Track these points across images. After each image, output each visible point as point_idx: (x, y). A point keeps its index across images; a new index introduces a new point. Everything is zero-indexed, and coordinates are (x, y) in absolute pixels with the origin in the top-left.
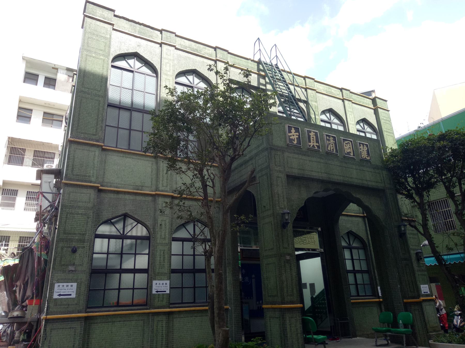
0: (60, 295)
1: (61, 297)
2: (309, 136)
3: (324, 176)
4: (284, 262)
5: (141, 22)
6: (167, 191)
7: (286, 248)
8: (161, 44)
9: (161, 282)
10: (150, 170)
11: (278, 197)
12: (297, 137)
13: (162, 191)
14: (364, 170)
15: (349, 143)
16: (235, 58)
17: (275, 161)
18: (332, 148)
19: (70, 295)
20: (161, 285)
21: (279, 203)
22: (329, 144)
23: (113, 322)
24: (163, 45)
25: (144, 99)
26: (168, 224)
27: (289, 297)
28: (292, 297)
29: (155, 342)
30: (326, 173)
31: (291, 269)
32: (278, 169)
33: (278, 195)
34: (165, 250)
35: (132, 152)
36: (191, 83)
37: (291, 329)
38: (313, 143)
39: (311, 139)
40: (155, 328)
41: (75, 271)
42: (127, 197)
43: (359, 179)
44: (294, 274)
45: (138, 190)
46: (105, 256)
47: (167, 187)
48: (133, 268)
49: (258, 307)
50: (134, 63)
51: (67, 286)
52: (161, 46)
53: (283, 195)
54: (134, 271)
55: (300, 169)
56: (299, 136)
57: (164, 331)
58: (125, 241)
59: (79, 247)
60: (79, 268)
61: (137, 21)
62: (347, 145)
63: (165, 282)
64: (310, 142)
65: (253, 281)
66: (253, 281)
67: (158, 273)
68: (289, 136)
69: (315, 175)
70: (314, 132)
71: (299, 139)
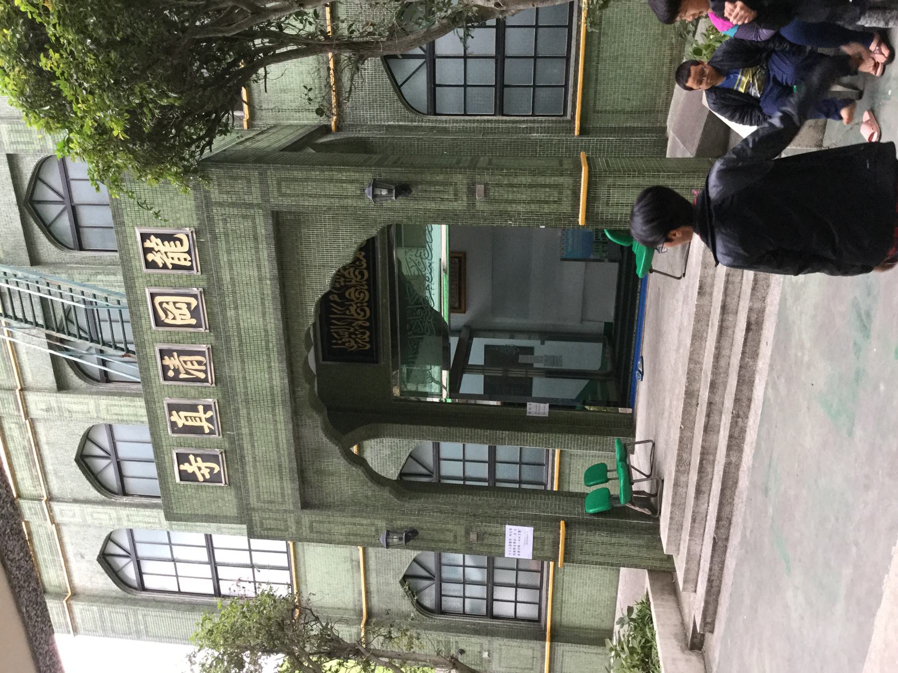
2: (187, 429)
3: (282, 415)
4: (482, 545)
7: (455, 537)
12: (199, 459)
15: (161, 304)
25: (113, 336)
27: (546, 547)
28: (546, 542)
30: (273, 409)
32: (294, 528)
33: (349, 534)
37: (601, 555)
39: (190, 423)
41: (489, 651)
42: (373, 580)
59: (457, 647)
60: (486, 647)
62: (171, 316)
69: (284, 435)
70: (171, 415)
71: (206, 458)
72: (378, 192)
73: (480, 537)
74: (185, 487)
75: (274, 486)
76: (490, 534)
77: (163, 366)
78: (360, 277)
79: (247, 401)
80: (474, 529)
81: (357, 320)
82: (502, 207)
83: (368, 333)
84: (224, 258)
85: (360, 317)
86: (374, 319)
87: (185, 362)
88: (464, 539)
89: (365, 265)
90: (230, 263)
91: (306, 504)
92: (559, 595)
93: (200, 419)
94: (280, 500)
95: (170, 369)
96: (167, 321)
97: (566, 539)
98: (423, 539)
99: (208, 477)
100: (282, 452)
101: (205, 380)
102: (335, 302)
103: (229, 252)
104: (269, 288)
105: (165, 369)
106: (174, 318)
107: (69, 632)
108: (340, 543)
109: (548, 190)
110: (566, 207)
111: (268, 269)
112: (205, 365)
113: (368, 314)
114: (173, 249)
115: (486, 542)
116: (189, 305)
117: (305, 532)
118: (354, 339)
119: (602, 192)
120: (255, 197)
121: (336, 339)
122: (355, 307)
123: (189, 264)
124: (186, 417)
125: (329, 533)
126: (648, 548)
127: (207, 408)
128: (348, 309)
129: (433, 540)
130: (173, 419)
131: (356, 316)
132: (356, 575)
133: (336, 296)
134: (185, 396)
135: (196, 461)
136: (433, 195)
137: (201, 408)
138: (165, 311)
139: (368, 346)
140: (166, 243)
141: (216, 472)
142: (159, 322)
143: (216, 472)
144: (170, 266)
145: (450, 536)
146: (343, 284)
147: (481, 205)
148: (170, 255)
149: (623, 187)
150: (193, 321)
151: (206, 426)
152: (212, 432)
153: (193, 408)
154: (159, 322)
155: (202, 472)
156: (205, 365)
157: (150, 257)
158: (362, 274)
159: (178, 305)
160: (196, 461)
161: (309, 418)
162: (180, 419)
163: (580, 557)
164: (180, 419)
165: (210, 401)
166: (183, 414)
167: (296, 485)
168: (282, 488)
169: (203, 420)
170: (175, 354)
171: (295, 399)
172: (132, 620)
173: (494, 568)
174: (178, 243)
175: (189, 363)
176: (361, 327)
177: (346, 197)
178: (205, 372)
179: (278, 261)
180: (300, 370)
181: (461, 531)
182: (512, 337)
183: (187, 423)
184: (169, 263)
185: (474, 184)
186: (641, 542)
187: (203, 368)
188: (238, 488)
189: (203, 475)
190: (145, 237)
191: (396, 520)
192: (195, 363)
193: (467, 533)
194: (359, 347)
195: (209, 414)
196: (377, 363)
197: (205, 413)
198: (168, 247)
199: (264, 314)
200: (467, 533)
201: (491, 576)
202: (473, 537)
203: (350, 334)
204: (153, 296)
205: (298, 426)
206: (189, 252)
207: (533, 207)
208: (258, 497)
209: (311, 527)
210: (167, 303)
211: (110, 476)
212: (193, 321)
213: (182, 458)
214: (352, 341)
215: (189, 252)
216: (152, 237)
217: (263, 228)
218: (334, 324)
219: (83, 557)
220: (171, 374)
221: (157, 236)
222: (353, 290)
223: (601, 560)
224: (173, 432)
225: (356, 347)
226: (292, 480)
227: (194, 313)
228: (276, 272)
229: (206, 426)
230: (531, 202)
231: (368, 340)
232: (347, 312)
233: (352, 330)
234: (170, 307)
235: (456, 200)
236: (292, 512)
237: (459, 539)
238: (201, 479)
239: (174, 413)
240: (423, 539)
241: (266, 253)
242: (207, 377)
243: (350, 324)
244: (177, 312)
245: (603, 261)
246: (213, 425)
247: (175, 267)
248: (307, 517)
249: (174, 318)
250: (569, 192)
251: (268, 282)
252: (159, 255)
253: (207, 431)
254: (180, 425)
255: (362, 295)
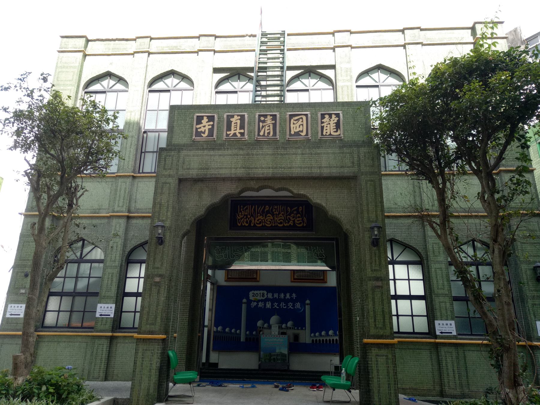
0: (11, 315)
1: (13, 316)
3: (241, 172)
4: (151, 284)
5: (114, 38)
6: (122, 212)
7: (158, 268)
8: (404, 46)
9: (106, 305)
10: (109, 191)
11: (160, 208)
12: (210, 127)
13: (117, 212)
14: (319, 154)
15: (302, 118)
16: (143, 49)
17: (165, 164)
18: (267, 132)
19: (19, 315)
20: (106, 309)
21: (159, 215)
22: (263, 127)
23: (58, 342)
24: (336, 49)
26: (119, 246)
28: (153, 326)
29: (93, 365)
30: (244, 168)
31: (158, 293)
32: (166, 173)
33: (160, 204)
34: (113, 273)
35: (147, 175)
36: (376, 82)
37: (142, 363)
38: (235, 130)
39: (233, 125)
40: (95, 351)
43: (306, 168)
44: (162, 299)
45: (95, 213)
46: (63, 279)
47: (123, 206)
48: (409, 294)
49: (313, 340)
50: (171, 81)
51: (18, 307)
52: (405, 48)
53: (168, 205)
54: (410, 297)
55: (201, 169)
56: (213, 126)
57: (104, 355)
58: (93, 264)
61: (111, 38)
62: (295, 122)
63: (110, 305)
64: (230, 130)
65: (308, 308)
66: (308, 308)
67: (104, 296)
68: (197, 129)
69: (225, 173)
70: (238, 116)
71: (211, 131)
72: (376, 229)
73: (157, 284)
74: (193, 118)
75: (193, 163)
76: (159, 290)
77: (267, 115)
78: (279, 222)
79: (248, 154)
80: (162, 280)
81: (255, 220)
82: (370, 295)
83: (247, 225)
84: (330, 151)
85: (256, 220)
86: (255, 228)
87: (269, 126)
88: (156, 273)
89: (285, 225)
90: (328, 153)
91: (180, 181)
92: (64, 340)
93: (235, 130)
94: (185, 167)
95: (265, 118)
96: (292, 120)
97: (155, 339)
98: (156, 248)
99: (199, 130)
100: (217, 170)
101: (259, 135)
102: (264, 208)
103: (334, 153)
104: (316, 171)
105: (265, 116)
106: (294, 124)
107: (60, 48)
108: (155, 199)
109: (382, 321)
110: (373, 331)
111: (326, 172)
112: (268, 136)
113: (279, 225)
114: (332, 128)
115: (154, 287)
116: (302, 131)
117: (163, 180)
118: (243, 217)
119: (383, 352)
120: (364, 169)
121: (243, 208)
122: (262, 219)
123: (324, 134)
124: (237, 123)
125: (162, 193)
126: (148, 395)
127: (242, 134)
128: (261, 215)
129: (155, 254)
130: (236, 117)
131: (257, 219)
132: (89, 211)
133: (268, 209)
134: (249, 123)
135: (209, 125)
136: (374, 258)
137: (242, 131)
138: (298, 120)
139: (239, 225)
140: (335, 125)
141: (202, 135)
142: (291, 116)
143: (202, 135)
144: (323, 125)
145: (158, 265)
146: (275, 213)
147: (371, 284)
148: (329, 126)
149: (387, 363)
150: (292, 133)
151: (232, 132)
152: (227, 135)
153: (242, 127)
154: (291, 116)
155: (202, 128)
156: (268, 136)
157: (327, 116)
158: (281, 223)
159: (301, 126)
160: (209, 125)
161: (237, 187)
162: (235, 120)
163: (140, 350)
164: (235, 120)
165: (246, 137)
166: (239, 122)
167: (195, 176)
168: (193, 169)
169: (235, 132)
170: (274, 122)
171: (249, 180)
172: (68, 83)
173: (74, 297)
174: (335, 130)
175: (268, 128)
176: (251, 221)
177: (368, 213)
178: (264, 135)
179: (329, 177)
180: (266, 184)
181: (162, 271)
182: (210, 310)
183: (233, 123)
184: (325, 125)
185: (381, 280)
186: (151, 391)
187: (266, 134)
188: (191, 145)
189: (200, 128)
190: (338, 115)
191: (170, 232)
192: (269, 131)
193: (160, 276)
194: (239, 220)
195: (239, 135)
196: (230, 229)
197: (239, 133)
198: (333, 125)
199: (301, 168)
200: (160, 276)
201: (67, 294)
202: (157, 279)
203: (247, 215)
204: (306, 115)
205: (232, 180)
206: (330, 134)
207: (371, 313)
208: (188, 156)
209: (166, 183)
210: (302, 121)
211: (159, 85)
212: (292, 133)
213: (211, 119)
214: (242, 216)
215: (330, 134)
216: (337, 119)
217: (346, 172)
218: (252, 207)
219: (111, 64)
220: (262, 118)
221: (339, 121)
222: (272, 218)
223: (139, 363)
224: (228, 116)
225: (239, 218)
226: (197, 175)
227: (297, 134)
228: (325, 175)
229: (232, 132)
230: (374, 312)
231: (243, 224)
232: (259, 215)
233: (249, 216)
234: (300, 123)
235: (372, 271)
236: (177, 173)
237: (156, 270)
238: (198, 126)
239: (239, 117)
240: (156, 248)
241: (335, 172)
242: (261, 136)
243: (252, 215)
244: (298, 125)
245: (259, 360)
246: (232, 136)
247: (322, 128)
248: (173, 182)
249: (294, 124)
250: (381, 333)
251: (318, 171)
252: (328, 120)
253: (228, 133)
254: (231, 120)
255: (269, 223)
